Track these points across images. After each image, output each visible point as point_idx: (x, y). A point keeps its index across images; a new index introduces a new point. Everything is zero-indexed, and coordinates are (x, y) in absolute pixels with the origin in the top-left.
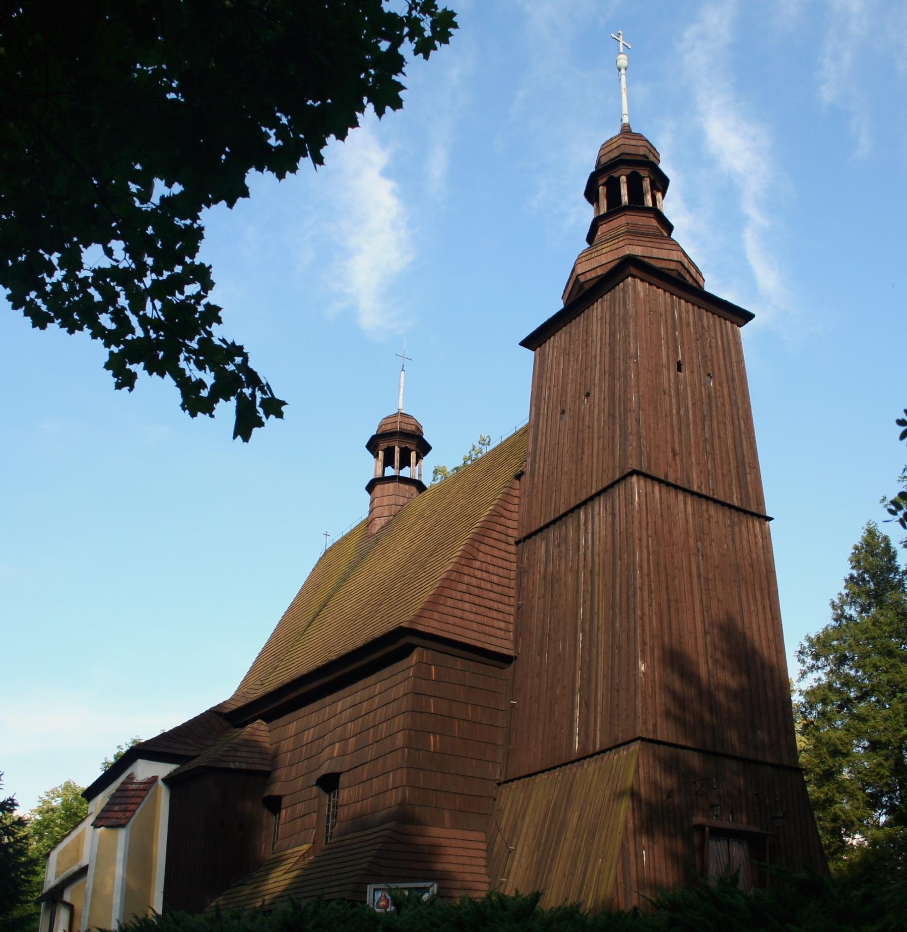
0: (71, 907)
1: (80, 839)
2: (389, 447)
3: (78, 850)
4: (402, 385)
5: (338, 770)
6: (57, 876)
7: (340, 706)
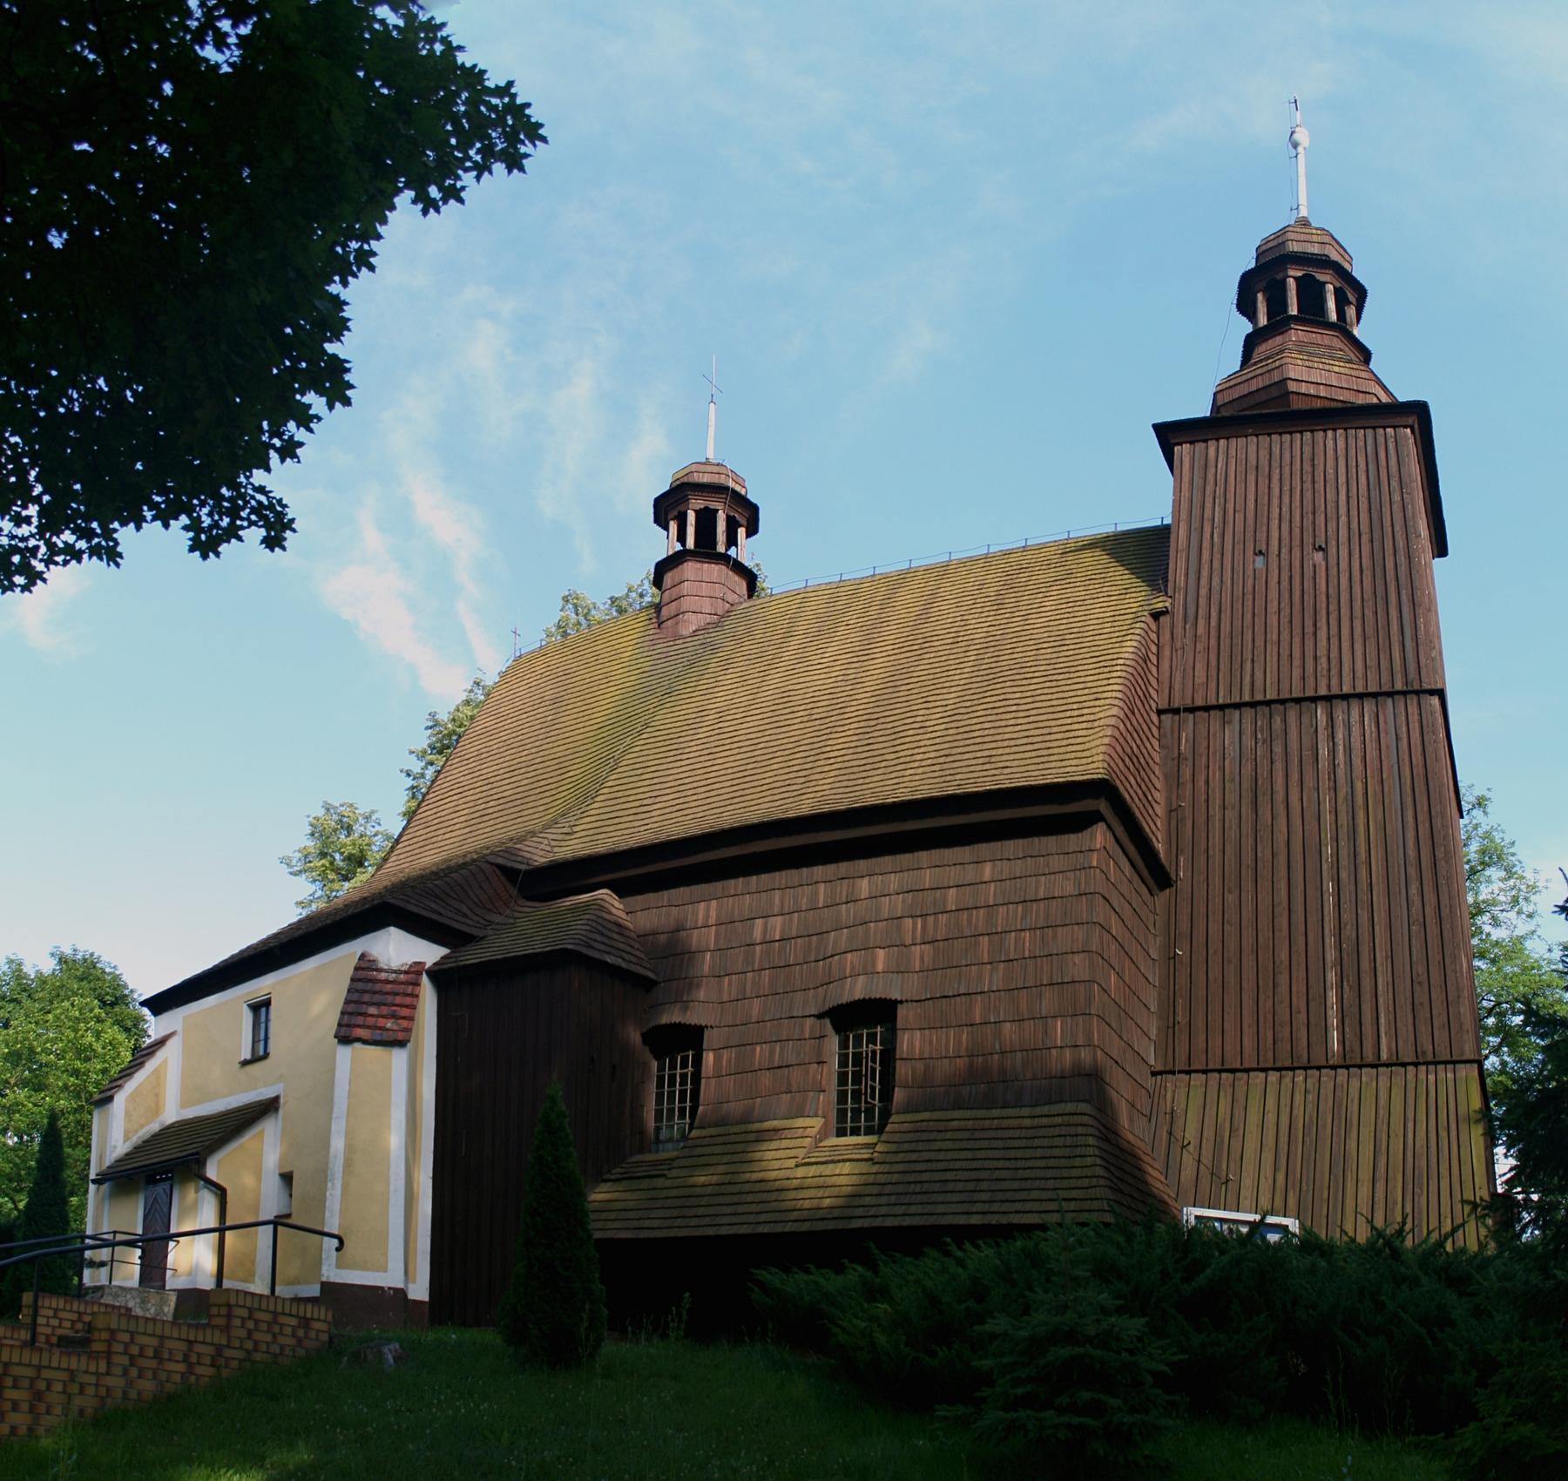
0: (221, 1193)
1: (158, 1074)
2: (706, 508)
3: (157, 1095)
4: (712, 423)
5: (896, 996)
6: (127, 1138)
7: (878, 885)
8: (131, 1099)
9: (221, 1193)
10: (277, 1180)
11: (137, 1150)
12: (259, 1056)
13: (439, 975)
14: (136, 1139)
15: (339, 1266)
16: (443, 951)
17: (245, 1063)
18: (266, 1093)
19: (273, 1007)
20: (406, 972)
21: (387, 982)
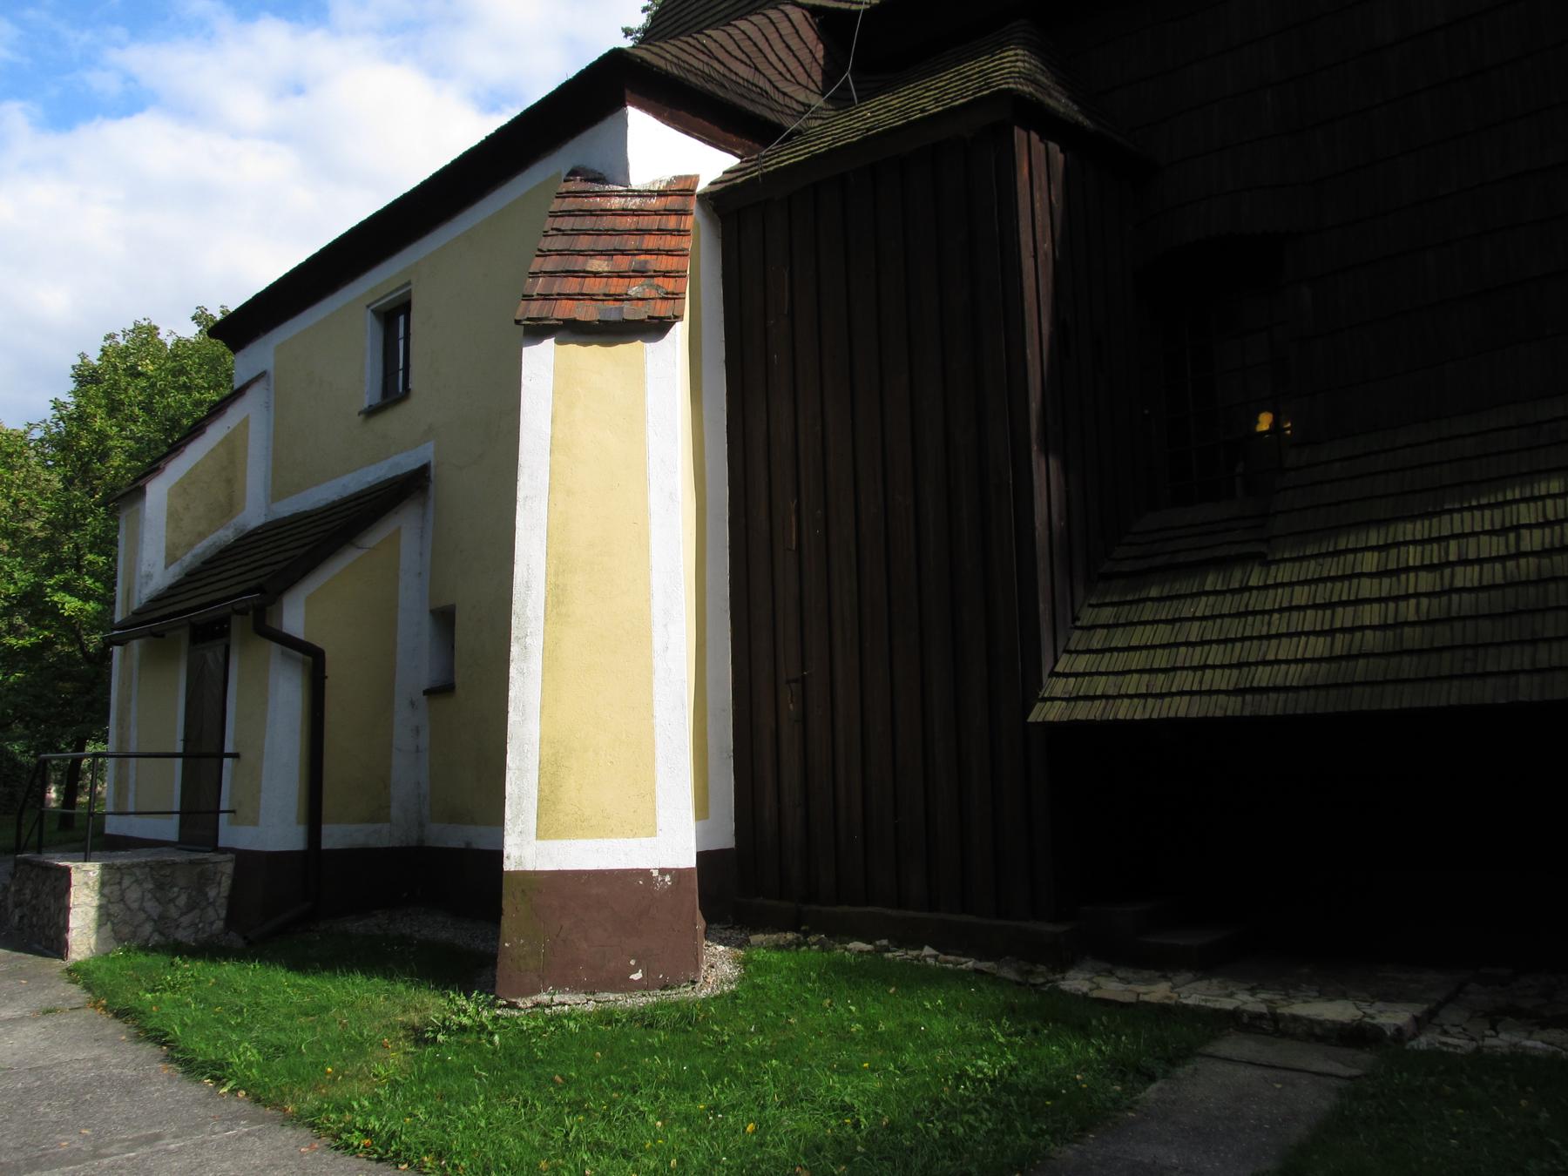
0: (313, 660)
1: (233, 448)
6: (171, 560)
8: (181, 489)
9: (313, 660)
10: (427, 621)
11: (192, 579)
12: (394, 388)
13: (724, 202)
14: (188, 559)
15: (541, 834)
17: (371, 412)
18: (406, 462)
20: (661, 194)
21: (624, 212)
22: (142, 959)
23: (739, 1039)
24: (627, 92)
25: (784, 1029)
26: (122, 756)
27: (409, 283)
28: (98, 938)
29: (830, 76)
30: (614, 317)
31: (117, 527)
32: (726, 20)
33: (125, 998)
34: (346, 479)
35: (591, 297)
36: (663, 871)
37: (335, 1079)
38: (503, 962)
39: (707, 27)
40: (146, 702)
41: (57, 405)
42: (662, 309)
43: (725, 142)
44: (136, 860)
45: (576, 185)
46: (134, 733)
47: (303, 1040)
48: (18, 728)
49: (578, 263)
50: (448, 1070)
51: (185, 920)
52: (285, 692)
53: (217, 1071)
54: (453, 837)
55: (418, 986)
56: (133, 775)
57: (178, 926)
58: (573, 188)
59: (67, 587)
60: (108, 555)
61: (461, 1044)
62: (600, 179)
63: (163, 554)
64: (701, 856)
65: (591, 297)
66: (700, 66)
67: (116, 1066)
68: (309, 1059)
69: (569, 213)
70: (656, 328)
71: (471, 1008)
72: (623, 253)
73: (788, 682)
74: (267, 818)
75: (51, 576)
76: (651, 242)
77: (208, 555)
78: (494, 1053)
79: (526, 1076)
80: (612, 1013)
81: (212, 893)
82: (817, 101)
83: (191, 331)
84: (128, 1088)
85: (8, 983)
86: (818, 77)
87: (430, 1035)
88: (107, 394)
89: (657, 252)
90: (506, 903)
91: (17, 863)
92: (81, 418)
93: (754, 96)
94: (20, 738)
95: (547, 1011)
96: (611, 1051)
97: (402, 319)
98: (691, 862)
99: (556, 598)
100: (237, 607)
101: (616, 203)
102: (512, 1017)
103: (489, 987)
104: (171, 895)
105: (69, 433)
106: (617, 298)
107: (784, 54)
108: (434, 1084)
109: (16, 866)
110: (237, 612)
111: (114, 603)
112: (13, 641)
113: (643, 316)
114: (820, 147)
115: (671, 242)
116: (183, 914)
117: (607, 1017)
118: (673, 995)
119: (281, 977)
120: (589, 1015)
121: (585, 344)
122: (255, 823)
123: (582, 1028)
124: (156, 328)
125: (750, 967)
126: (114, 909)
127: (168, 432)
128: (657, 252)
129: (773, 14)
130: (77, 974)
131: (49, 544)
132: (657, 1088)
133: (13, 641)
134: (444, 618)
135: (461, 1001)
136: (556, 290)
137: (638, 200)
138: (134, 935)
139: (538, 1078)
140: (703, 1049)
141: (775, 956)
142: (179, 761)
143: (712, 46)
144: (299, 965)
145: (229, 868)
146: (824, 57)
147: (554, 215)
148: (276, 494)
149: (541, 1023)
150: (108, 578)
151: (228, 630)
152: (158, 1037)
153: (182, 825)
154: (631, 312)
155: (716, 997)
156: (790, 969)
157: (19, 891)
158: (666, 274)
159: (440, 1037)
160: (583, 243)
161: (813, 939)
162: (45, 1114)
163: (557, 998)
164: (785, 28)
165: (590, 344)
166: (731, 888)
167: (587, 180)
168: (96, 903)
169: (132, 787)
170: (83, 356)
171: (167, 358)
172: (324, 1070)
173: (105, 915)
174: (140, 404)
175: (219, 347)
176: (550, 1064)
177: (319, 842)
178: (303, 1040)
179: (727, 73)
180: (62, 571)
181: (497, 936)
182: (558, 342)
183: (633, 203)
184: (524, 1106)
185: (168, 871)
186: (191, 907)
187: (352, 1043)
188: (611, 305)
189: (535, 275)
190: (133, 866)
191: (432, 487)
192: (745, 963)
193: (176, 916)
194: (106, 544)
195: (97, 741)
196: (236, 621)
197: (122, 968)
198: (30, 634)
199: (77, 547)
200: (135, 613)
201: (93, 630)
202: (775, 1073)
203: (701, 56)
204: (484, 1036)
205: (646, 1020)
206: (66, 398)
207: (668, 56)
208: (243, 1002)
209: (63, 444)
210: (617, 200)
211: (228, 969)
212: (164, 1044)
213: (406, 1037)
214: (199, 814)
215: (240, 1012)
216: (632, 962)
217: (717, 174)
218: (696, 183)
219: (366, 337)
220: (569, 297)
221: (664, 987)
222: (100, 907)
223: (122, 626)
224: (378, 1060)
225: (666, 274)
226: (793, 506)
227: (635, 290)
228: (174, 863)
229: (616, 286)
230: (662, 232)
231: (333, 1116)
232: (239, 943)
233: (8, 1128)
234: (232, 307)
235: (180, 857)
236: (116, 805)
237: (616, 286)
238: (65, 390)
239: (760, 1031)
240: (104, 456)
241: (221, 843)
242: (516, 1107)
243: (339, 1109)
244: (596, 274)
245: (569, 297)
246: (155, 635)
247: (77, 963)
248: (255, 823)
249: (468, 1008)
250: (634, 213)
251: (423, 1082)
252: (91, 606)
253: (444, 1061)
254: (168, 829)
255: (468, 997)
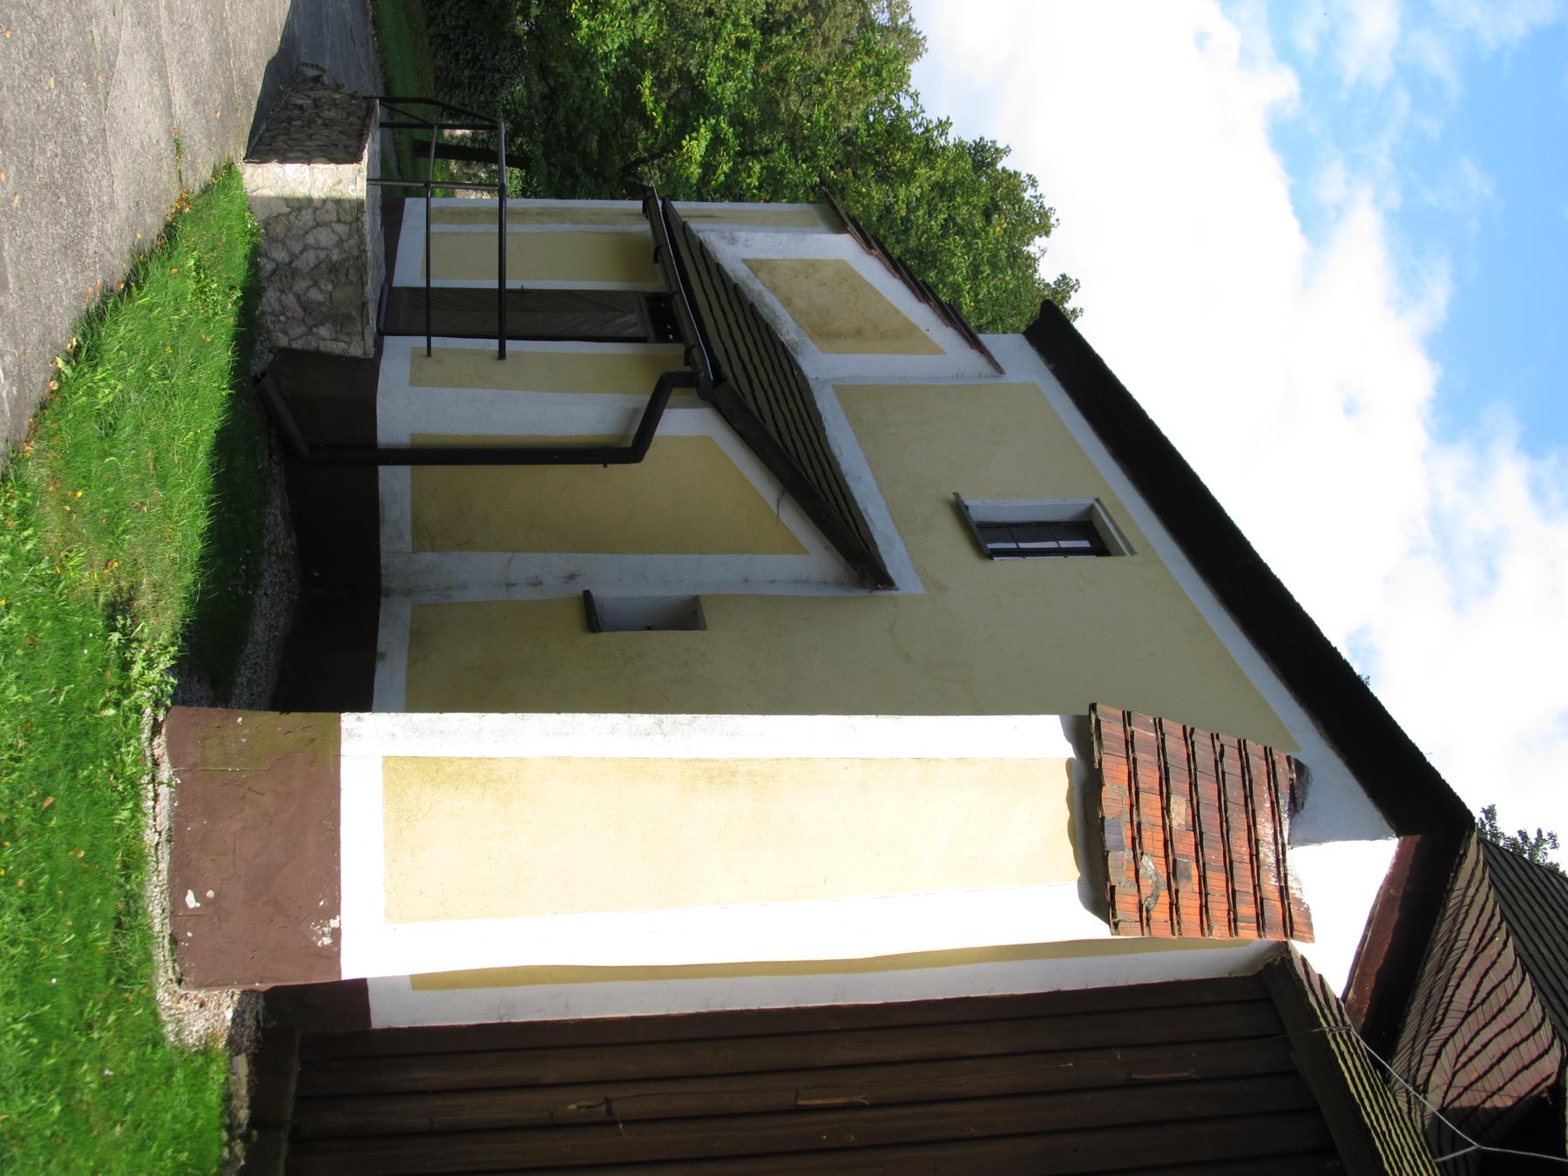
0: (631, 447)
3: (858, 333)
6: (755, 266)
8: (845, 275)
10: (683, 591)
11: (732, 293)
12: (992, 537)
13: (1277, 980)
14: (756, 287)
15: (392, 765)
16: (1337, 984)
17: (959, 510)
19: (1092, 560)
20: (1284, 891)
21: (1254, 843)
22: (242, 250)
23: (97, 1052)
24: (1417, 838)
25: (107, 1117)
26: (501, 215)
27: (1132, 552)
28: (270, 199)
29: (1473, 1120)
30: (1110, 838)
31: (794, 200)
32: (1527, 962)
33: (190, 234)
34: (868, 478)
35: (1134, 805)
36: (336, 934)
37: (66, 502)
38: (217, 714)
39: (1532, 975)
40: (569, 241)
41: (943, 126)
42: (1125, 904)
43: (1362, 973)
44: (368, 239)
45: (1284, 774)
46: (532, 228)
47: (121, 457)
48: (539, 88)
49: (1179, 783)
50: (67, 651)
51: (290, 300)
52: (589, 414)
53: (86, 353)
54: (392, 637)
55: (190, 601)
56: (475, 230)
57: (282, 291)
58: (1279, 770)
59: (717, 141)
60: (759, 188)
61: (105, 666)
62: (1295, 805)
63: (761, 256)
64: (360, 986)
65: (1134, 805)
66: (1464, 936)
67: (102, 230)
68: (95, 467)
69: (1245, 767)
70: (1100, 898)
71: (153, 675)
72: (1199, 845)
73: (608, 1101)
74: (421, 395)
75: (731, 124)
76: (1216, 881)
77: (763, 311)
78: (91, 710)
79: (54, 758)
80: (139, 868)
81: (324, 331)
82: (1432, 1103)
83: (1047, 273)
84: (72, 247)
85: (218, 97)
86: (1467, 1101)
87: (120, 621)
88: (959, 182)
89: (1203, 892)
90: (297, 718)
91: (368, 99)
92: (928, 153)
93: (1430, 1012)
94: (530, 92)
95: (146, 778)
96: (85, 871)
97: (1085, 544)
98: (349, 972)
99: (718, 774)
100: (695, 351)
101: (1265, 830)
102: (141, 731)
103: (182, 698)
104: (322, 284)
105: (909, 139)
106: (1136, 842)
107: (1494, 1050)
108: (51, 634)
109: (365, 98)
110: (688, 352)
111: (701, 199)
112: (647, 83)
113: (1114, 880)
114: (1371, 1115)
115: (1219, 909)
116: (298, 297)
117: (133, 862)
118: (162, 954)
119: (209, 422)
120: (138, 836)
121: (1070, 800)
122: (414, 381)
123: (120, 829)
124: (1047, 234)
125: (200, 1060)
126: (307, 216)
127: (920, 255)
128: (1203, 892)
129: (1546, 1033)
130: (227, 171)
131: (770, 120)
132: (27, 943)
133: (647, 83)
134: (687, 616)
135: (165, 662)
136: (1140, 756)
137: (1272, 859)
138: (273, 239)
139: (51, 774)
140: (81, 1002)
141: (213, 1097)
142: (495, 284)
143: (1492, 951)
144: (224, 444)
145: (355, 350)
146: (1495, 1108)
147: (1242, 746)
148: (844, 392)
149: (129, 771)
150: (732, 191)
151: (667, 341)
152: (135, 279)
153: (413, 291)
154: (1119, 862)
155: (155, 1014)
156: (192, 1123)
157: (334, 104)
158: (1174, 906)
159: (116, 636)
160: (1207, 789)
161: (239, 1147)
162: (43, 152)
163: (164, 791)
164: (1529, 1050)
165: (1071, 808)
166: (314, 1037)
167: (1292, 788)
168: (316, 194)
169: (464, 229)
170: (1007, 151)
171: (1012, 248)
172: (80, 487)
173: (299, 206)
174: (957, 229)
175: (1032, 310)
176: (70, 789)
177: (387, 463)
178: (121, 457)
179: (1457, 973)
180: (737, 136)
181: (252, 706)
182: (1069, 763)
183: (1267, 854)
184: (11, 758)
185: (353, 277)
186: (306, 306)
187: (113, 520)
188: (1127, 833)
189: (1158, 725)
190: (362, 237)
191: (862, 593)
192: (206, 1052)
193: (296, 288)
194: (774, 187)
195: (525, 180)
196: (679, 349)
197: (230, 228)
198: (656, 102)
199: (767, 152)
200: (684, 227)
201: (667, 174)
202: (40, 1112)
203: (1477, 935)
204: (114, 694)
205: (127, 919)
206: (952, 136)
207: (1472, 890)
208: (178, 380)
209: (896, 132)
210: (1270, 832)
211: (223, 356)
212: (127, 285)
213: (120, 589)
214: (428, 312)
215: (164, 375)
216: (210, 894)
217: (1317, 967)
218: (1302, 939)
219: (1061, 502)
220: (1133, 775)
221: (174, 941)
222: (310, 200)
223: (667, 211)
224: (89, 556)
225: (1174, 906)
226: (859, 1099)
227: (1151, 865)
228: (363, 285)
229: (1153, 839)
230: (1232, 896)
231: (14, 504)
232: (257, 367)
233: (28, 109)
234: (1079, 325)
235: (371, 291)
236: (441, 211)
237: (1153, 839)
238: (963, 132)
239: (105, 1084)
240: (882, 178)
241: (388, 340)
242: (11, 746)
243: (24, 512)
244: (1166, 810)
245: (1133, 775)
246: (657, 251)
247: (239, 176)
248: (414, 381)
249: (154, 669)
250: (1254, 856)
251: (56, 618)
252: (695, 171)
253: (82, 644)
254: (409, 274)
255: (170, 670)
